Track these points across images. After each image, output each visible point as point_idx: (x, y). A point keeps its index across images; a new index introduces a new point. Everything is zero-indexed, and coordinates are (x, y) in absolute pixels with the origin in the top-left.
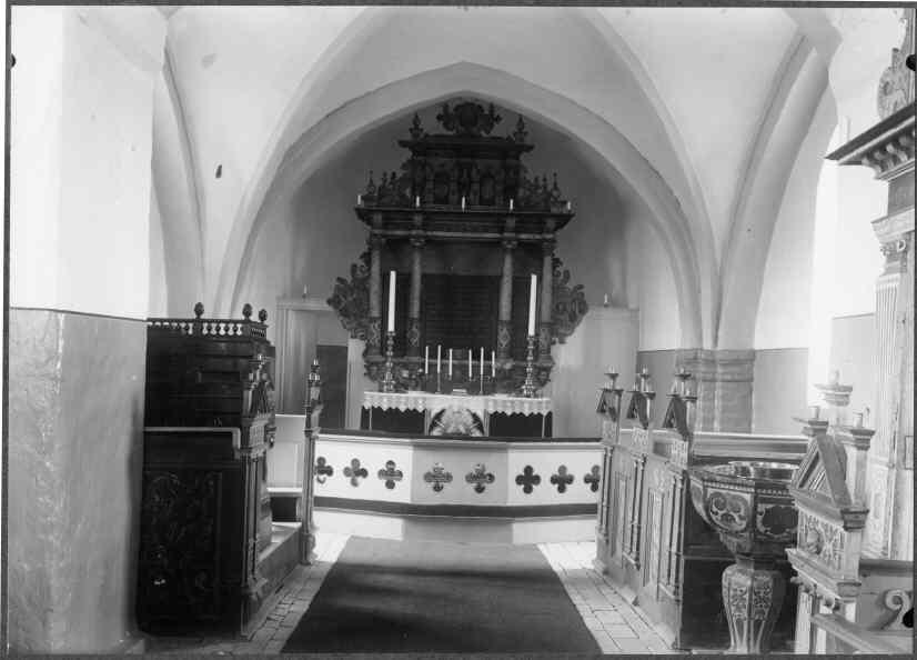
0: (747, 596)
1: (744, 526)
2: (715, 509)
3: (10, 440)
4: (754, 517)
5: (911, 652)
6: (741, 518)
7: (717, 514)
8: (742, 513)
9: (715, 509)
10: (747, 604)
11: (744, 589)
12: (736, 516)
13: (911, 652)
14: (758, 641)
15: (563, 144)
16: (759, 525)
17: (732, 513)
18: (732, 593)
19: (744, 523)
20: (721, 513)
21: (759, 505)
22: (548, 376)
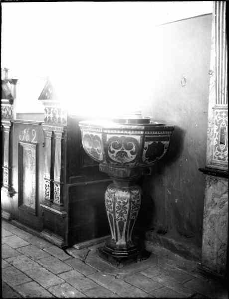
0: (127, 206)
1: (133, 158)
2: (112, 149)
3: (189, 20)
4: (142, 151)
5: (3, 4)
6: (132, 153)
7: (113, 152)
8: (134, 149)
9: (112, 149)
10: (127, 210)
11: (126, 201)
12: (128, 152)
13: (3, 4)
14: (131, 235)
15: (176, 127)
16: (144, 156)
17: (125, 150)
18: (117, 205)
19: (134, 157)
20: (117, 151)
21: (145, 142)
22: (31, 126)
